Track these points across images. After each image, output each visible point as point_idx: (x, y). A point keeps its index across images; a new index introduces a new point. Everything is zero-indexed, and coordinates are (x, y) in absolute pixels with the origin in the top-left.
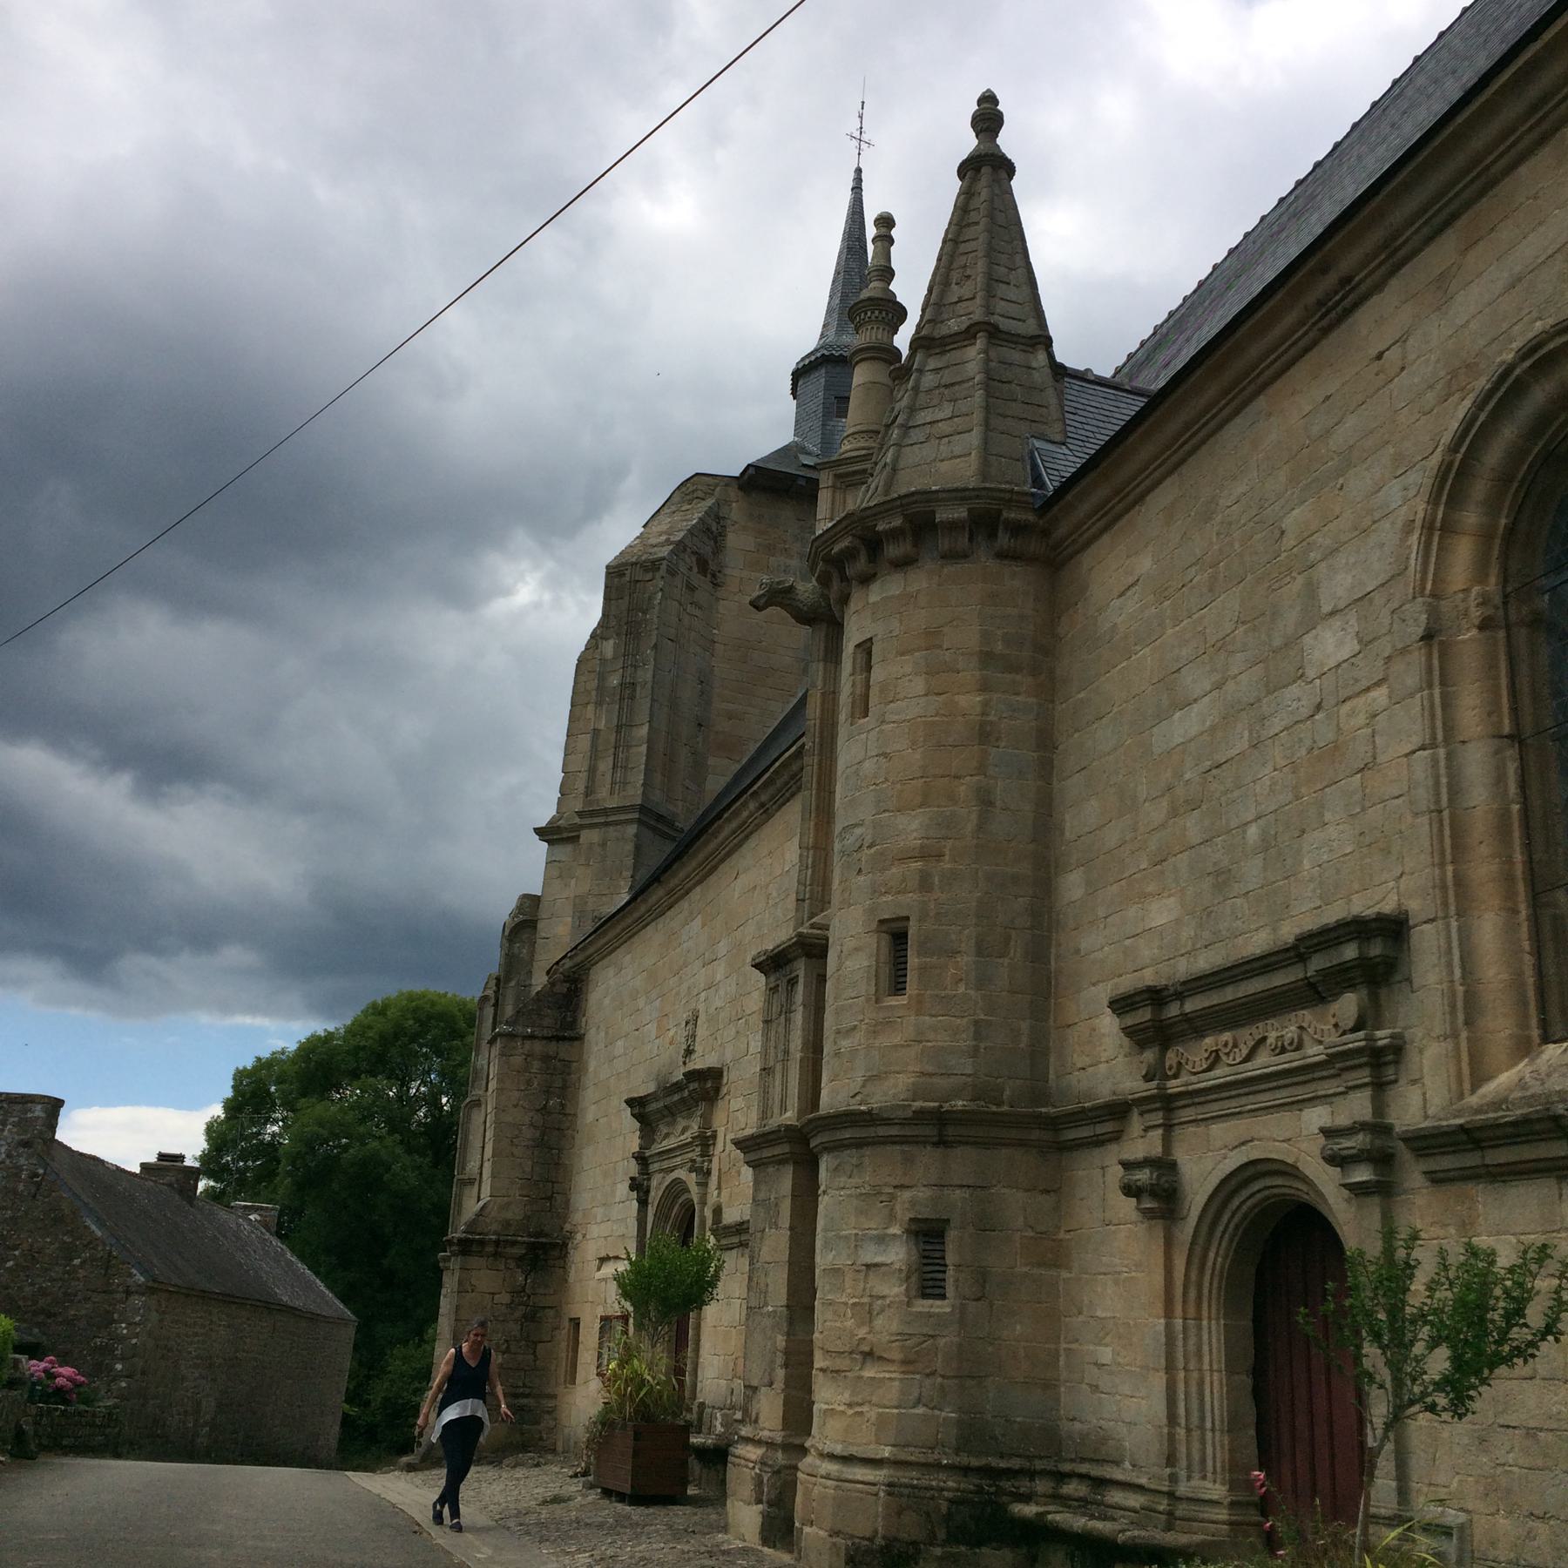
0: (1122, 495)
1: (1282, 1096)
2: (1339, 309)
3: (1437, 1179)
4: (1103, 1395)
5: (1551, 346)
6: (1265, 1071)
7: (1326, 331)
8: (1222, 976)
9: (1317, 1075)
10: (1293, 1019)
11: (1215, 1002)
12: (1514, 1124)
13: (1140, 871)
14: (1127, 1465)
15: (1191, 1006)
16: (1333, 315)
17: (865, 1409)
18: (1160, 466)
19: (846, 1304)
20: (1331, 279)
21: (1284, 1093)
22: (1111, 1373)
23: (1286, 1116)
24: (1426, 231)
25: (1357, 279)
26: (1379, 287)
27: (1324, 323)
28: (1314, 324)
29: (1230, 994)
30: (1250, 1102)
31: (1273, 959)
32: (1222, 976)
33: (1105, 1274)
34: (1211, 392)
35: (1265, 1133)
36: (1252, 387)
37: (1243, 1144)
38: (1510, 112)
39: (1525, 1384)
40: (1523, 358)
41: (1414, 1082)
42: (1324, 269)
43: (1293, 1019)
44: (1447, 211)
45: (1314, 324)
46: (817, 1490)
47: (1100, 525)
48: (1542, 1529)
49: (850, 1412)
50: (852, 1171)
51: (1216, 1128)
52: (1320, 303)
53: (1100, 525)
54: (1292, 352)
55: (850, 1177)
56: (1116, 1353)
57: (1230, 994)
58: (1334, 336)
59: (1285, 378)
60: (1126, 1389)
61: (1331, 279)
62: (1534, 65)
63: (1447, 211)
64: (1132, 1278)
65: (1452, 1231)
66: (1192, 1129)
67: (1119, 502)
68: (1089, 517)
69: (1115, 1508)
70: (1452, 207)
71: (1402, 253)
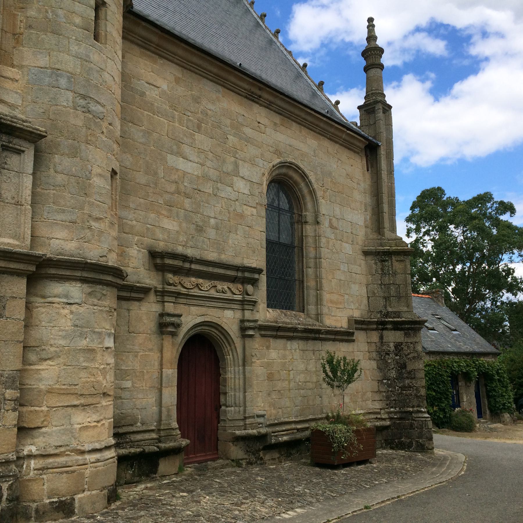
0: (157, 47)
1: (220, 305)
2: (253, 98)
3: (263, 336)
4: (124, 400)
5: (293, 166)
6: (220, 297)
7: (246, 97)
8: (206, 263)
10: (226, 284)
11: (205, 270)
13: (158, 203)
14: (139, 424)
15: (193, 266)
17: (103, 422)
18: (181, 61)
20: (259, 93)
21: (221, 304)
25: (261, 99)
26: (261, 105)
27: (248, 96)
28: (247, 93)
29: (210, 269)
30: (208, 304)
31: (231, 267)
32: (206, 263)
34: (215, 70)
36: (222, 83)
37: (202, 315)
38: (303, 115)
39: (279, 381)
40: (289, 163)
41: (258, 312)
42: (260, 89)
43: (226, 284)
45: (247, 93)
47: (140, 42)
48: (280, 410)
49: (99, 425)
50: (101, 297)
51: (193, 308)
52: (252, 93)
53: (140, 42)
54: (237, 90)
59: (228, 91)
61: (259, 93)
64: (146, 355)
65: (265, 348)
66: (182, 306)
67: (155, 48)
68: (139, 36)
69: (140, 441)
71: (270, 107)
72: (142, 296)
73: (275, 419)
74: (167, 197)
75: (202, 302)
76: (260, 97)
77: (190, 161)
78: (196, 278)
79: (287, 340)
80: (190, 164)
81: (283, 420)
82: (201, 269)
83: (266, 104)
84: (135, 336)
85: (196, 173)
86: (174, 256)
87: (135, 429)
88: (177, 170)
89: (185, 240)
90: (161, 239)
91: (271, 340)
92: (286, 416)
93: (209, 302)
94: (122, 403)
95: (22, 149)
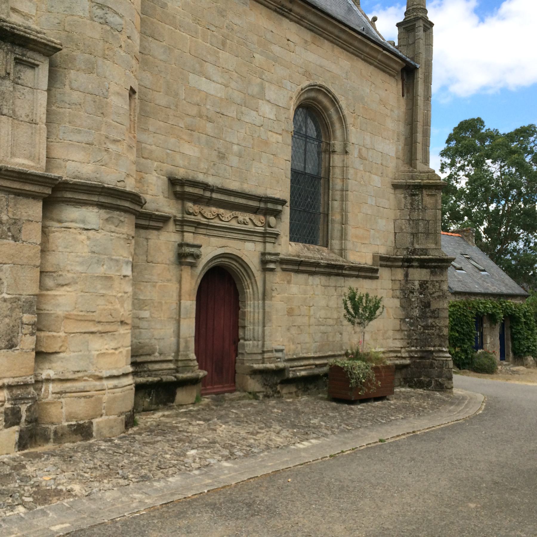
1: (241, 236)
3: (284, 270)
7: (275, 11)
9: (255, 234)
12: (311, 263)
15: (214, 196)
16: (281, 11)
19: (115, 296)
22: (148, 321)
23: (240, 243)
24: (308, 26)
26: (291, 20)
27: (278, 9)
29: (232, 199)
33: (146, 282)
35: (232, 246)
44: (314, 29)
46: (105, 398)
48: (299, 346)
51: (213, 240)
52: (282, 6)
55: (116, 227)
56: (151, 313)
57: (232, 199)
58: (275, 14)
60: (158, 326)
62: (344, 31)
63: (314, 29)
66: (202, 236)
70: (315, 30)
72: (160, 225)
73: (294, 354)
74: (188, 120)
75: (223, 233)
76: (291, 10)
77: (213, 81)
78: (216, 207)
79: (309, 275)
80: (213, 84)
81: (301, 355)
82: (222, 198)
83: (296, 19)
84: (153, 266)
85: (219, 95)
86: (195, 184)
87: (152, 358)
88: (199, 90)
89: (206, 167)
90: (182, 166)
91: (293, 274)
92: (305, 351)
93: (230, 234)
94: (140, 333)
95: (36, 62)
